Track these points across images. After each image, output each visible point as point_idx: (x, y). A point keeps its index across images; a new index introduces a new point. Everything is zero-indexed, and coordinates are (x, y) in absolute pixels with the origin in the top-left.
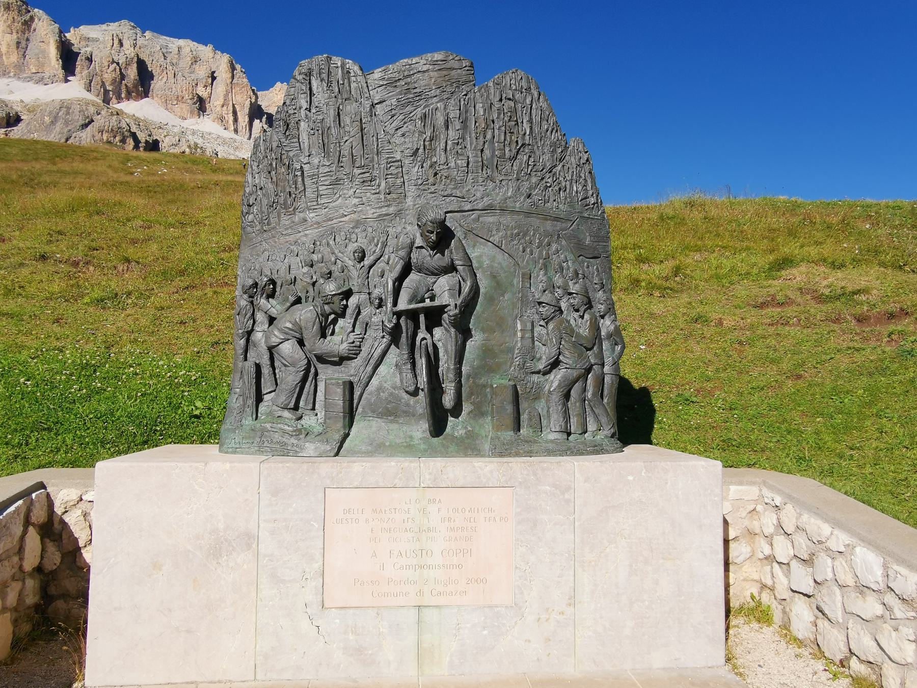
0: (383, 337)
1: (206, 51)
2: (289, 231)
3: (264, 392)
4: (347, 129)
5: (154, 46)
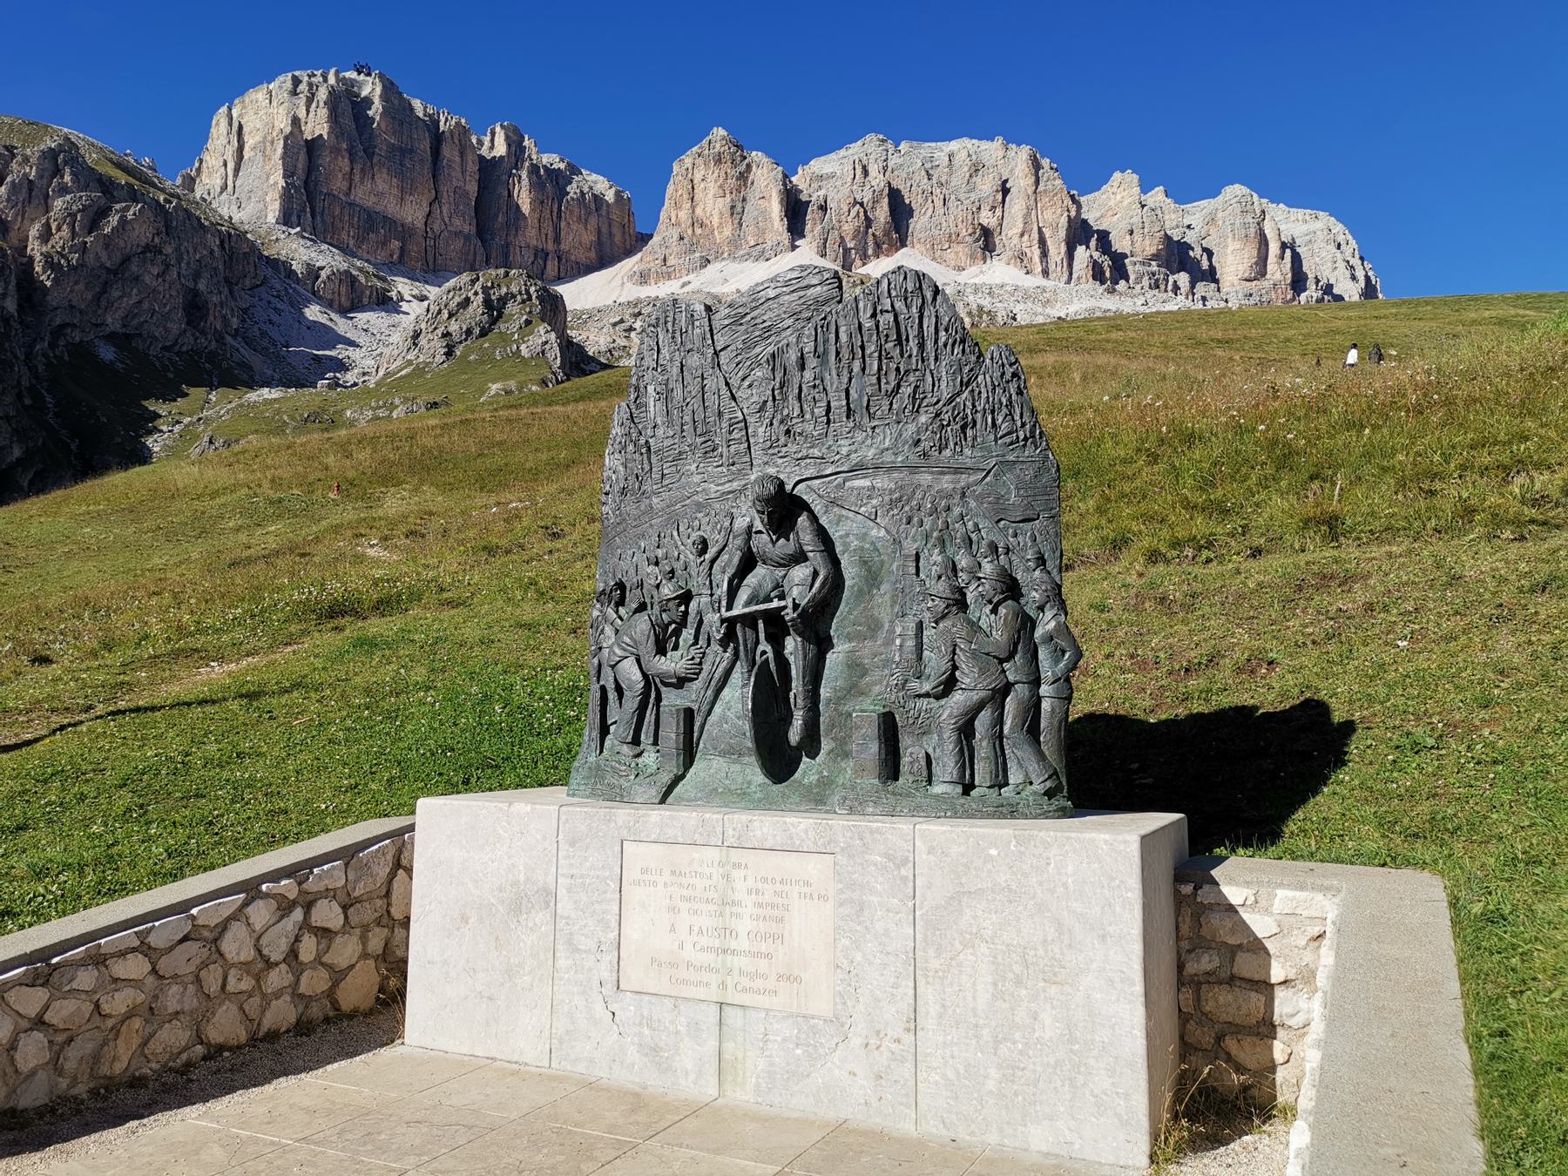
1: (991, 150)
5: (909, 163)
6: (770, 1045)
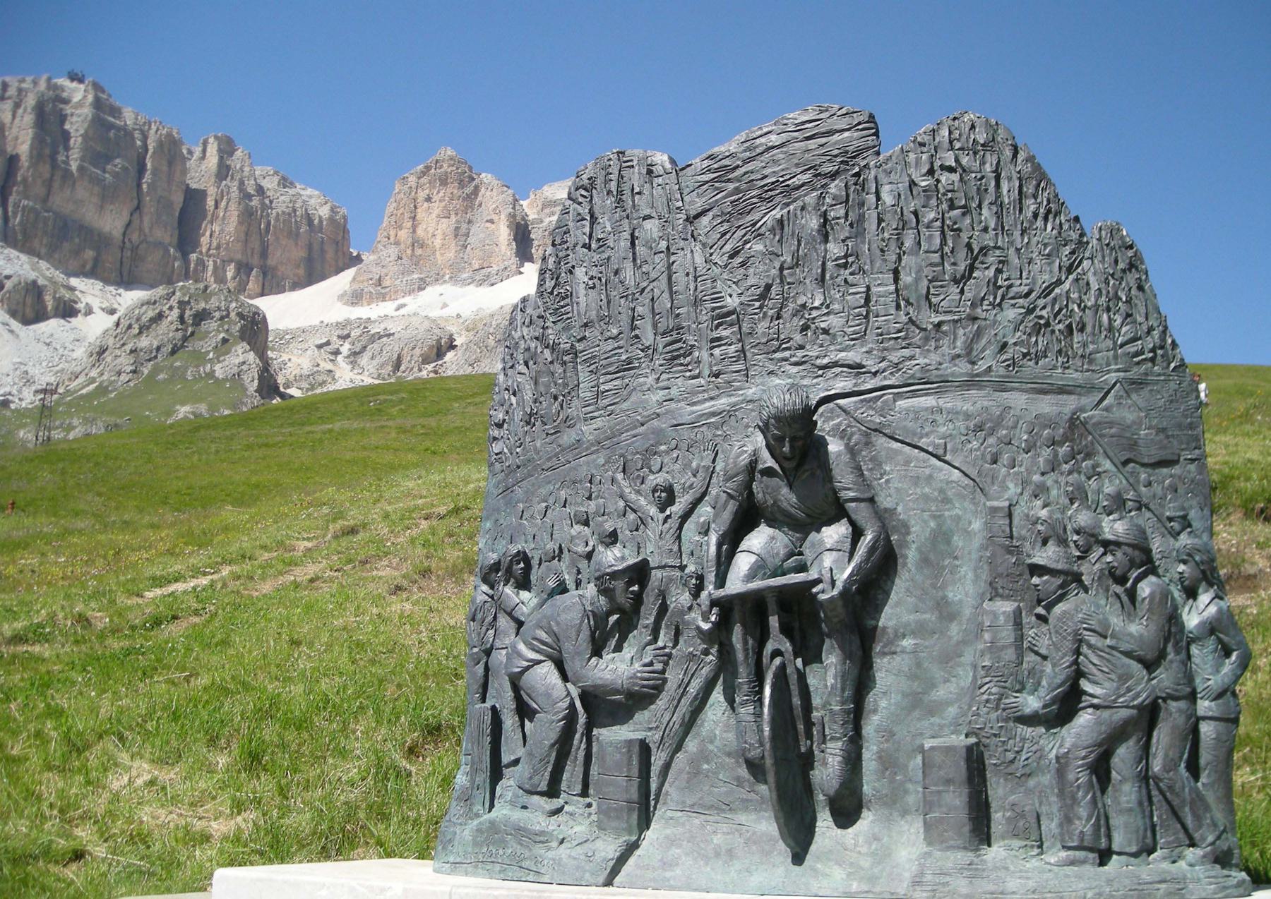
3: (506, 758)
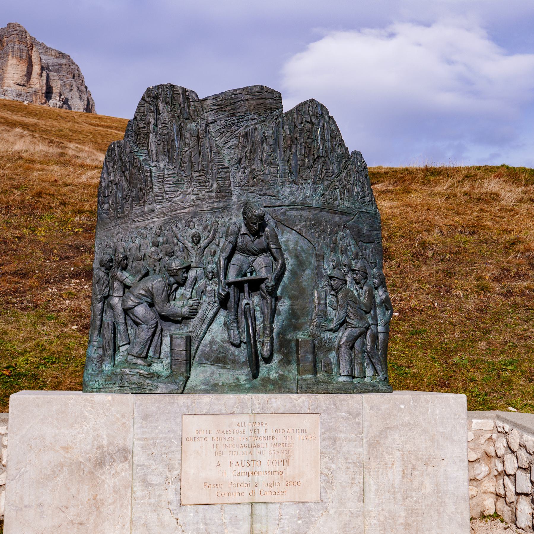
0: (215, 302)
2: (140, 218)
4: (187, 142)
6: (282, 521)
